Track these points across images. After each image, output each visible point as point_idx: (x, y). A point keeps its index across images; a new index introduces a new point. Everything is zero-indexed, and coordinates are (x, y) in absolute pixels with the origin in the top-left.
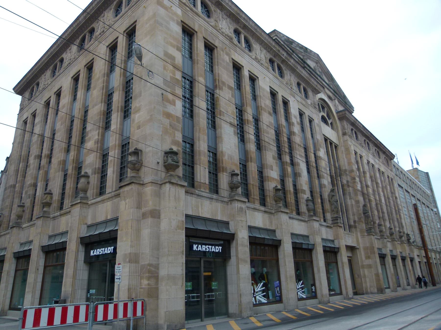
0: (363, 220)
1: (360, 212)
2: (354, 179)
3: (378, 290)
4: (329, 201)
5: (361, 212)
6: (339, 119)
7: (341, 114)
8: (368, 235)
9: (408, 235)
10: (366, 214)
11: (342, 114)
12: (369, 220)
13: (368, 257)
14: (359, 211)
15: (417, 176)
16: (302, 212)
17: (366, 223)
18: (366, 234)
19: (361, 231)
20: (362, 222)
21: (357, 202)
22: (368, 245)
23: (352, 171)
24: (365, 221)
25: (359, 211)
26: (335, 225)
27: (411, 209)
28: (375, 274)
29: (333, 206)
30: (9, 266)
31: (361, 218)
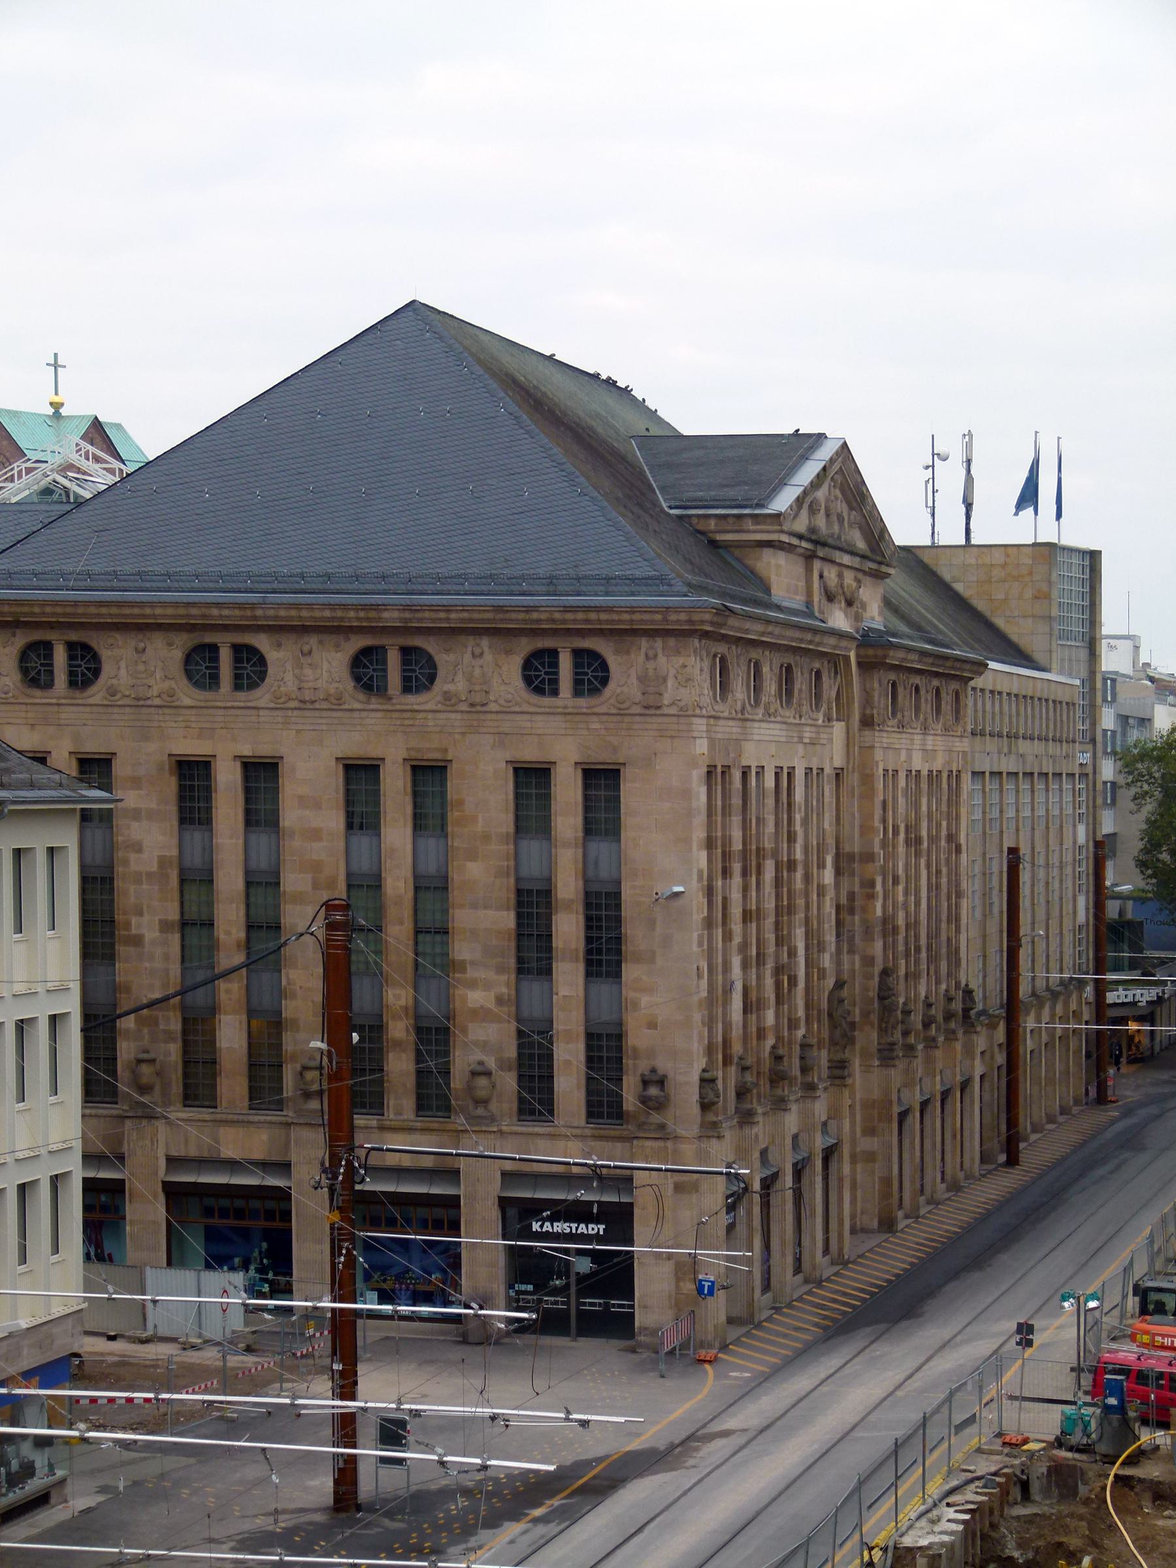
0: (874, 1018)
1: (871, 994)
2: (872, 884)
3: (880, 1223)
4: (830, 1015)
5: (873, 993)
6: (859, 664)
7: (871, 652)
8: (881, 1065)
9: (968, 992)
10: (887, 1002)
11: (876, 656)
12: (892, 1020)
13: (870, 1131)
14: (868, 990)
15: (1044, 587)
16: (576, 846)
17: (880, 1029)
18: (877, 1063)
19: (865, 1054)
20: (873, 1026)
21: (869, 961)
22: (876, 1094)
23: (869, 857)
24: (881, 1020)
25: (868, 990)
26: (837, 1082)
27: (999, 866)
28: (882, 1179)
29: (838, 1032)
30: (12, 1197)
31: (869, 1013)
